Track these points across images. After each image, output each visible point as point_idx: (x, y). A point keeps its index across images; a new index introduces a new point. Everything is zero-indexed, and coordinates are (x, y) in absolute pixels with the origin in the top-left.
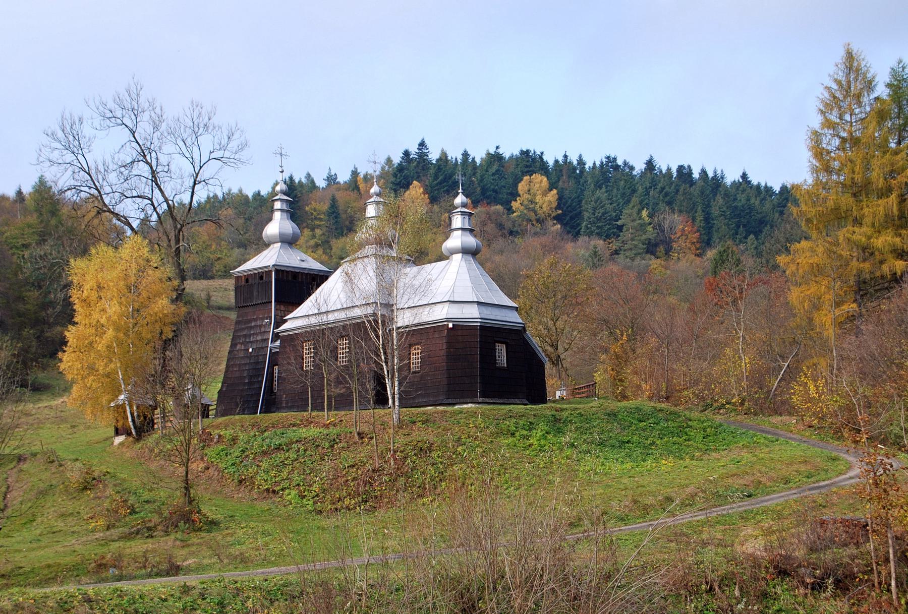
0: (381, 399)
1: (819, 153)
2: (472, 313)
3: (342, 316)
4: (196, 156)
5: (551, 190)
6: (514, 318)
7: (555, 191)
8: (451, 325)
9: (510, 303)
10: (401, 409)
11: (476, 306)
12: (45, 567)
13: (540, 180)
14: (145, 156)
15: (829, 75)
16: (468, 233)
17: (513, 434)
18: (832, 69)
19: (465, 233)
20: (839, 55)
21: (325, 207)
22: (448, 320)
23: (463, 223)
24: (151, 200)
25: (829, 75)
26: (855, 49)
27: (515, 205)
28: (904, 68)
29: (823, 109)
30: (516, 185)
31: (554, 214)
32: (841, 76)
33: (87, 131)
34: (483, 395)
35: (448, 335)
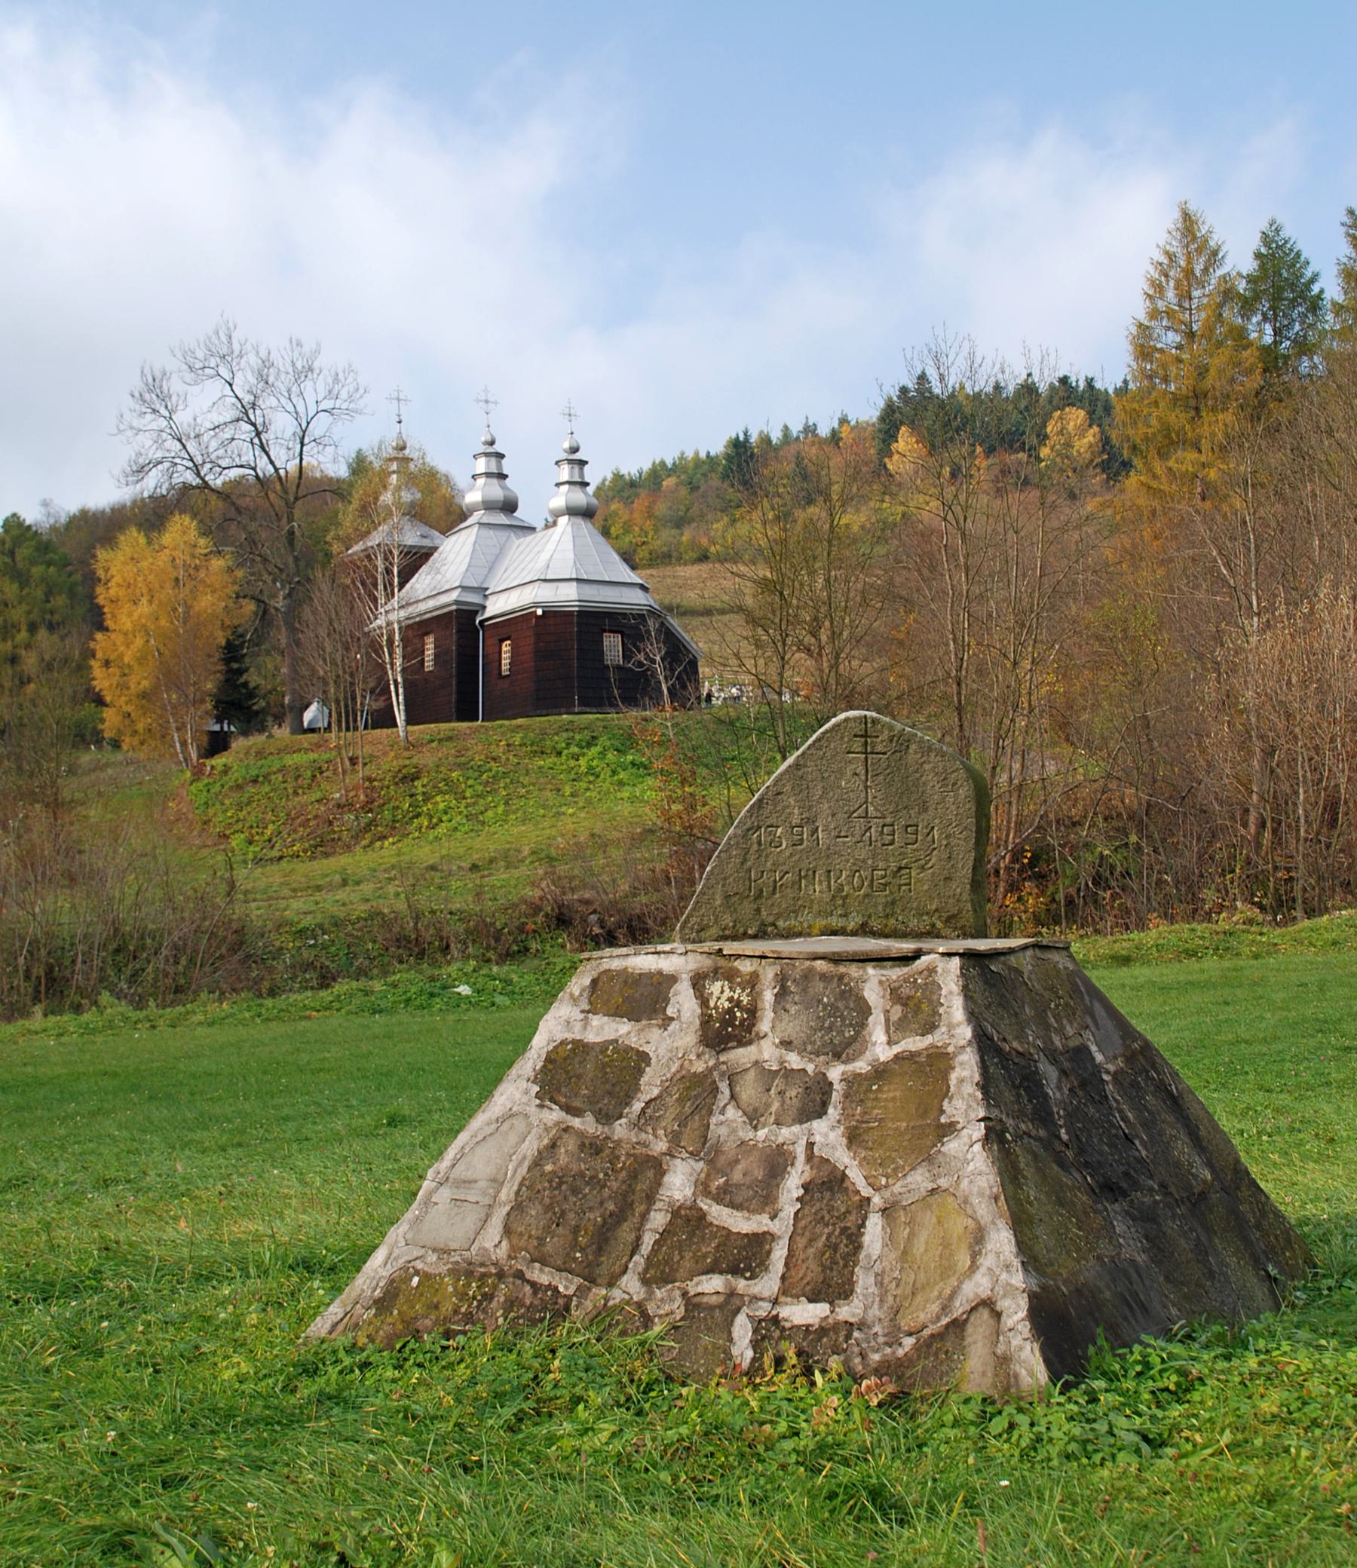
0: (384, 719)
1: (1144, 349)
2: (567, 595)
3: (431, 604)
4: (301, 409)
5: (1090, 426)
6: (636, 599)
7: (1096, 429)
8: (539, 612)
9: (634, 577)
10: (410, 728)
11: (575, 584)
12: (1136, 960)
13: (1076, 416)
14: (247, 414)
15: (1158, 246)
16: (577, 488)
17: (559, 754)
18: (1162, 238)
19: (573, 487)
20: (1171, 219)
21: (789, 467)
22: (536, 605)
23: (571, 474)
24: (254, 469)
25: (1158, 246)
26: (1192, 207)
27: (1044, 452)
28: (1277, 231)
29: (1151, 292)
30: (1044, 425)
31: (1097, 460)
32: (1175, 247)
33: (175, 386)
34: (583, 703)
35: (536, 625)
